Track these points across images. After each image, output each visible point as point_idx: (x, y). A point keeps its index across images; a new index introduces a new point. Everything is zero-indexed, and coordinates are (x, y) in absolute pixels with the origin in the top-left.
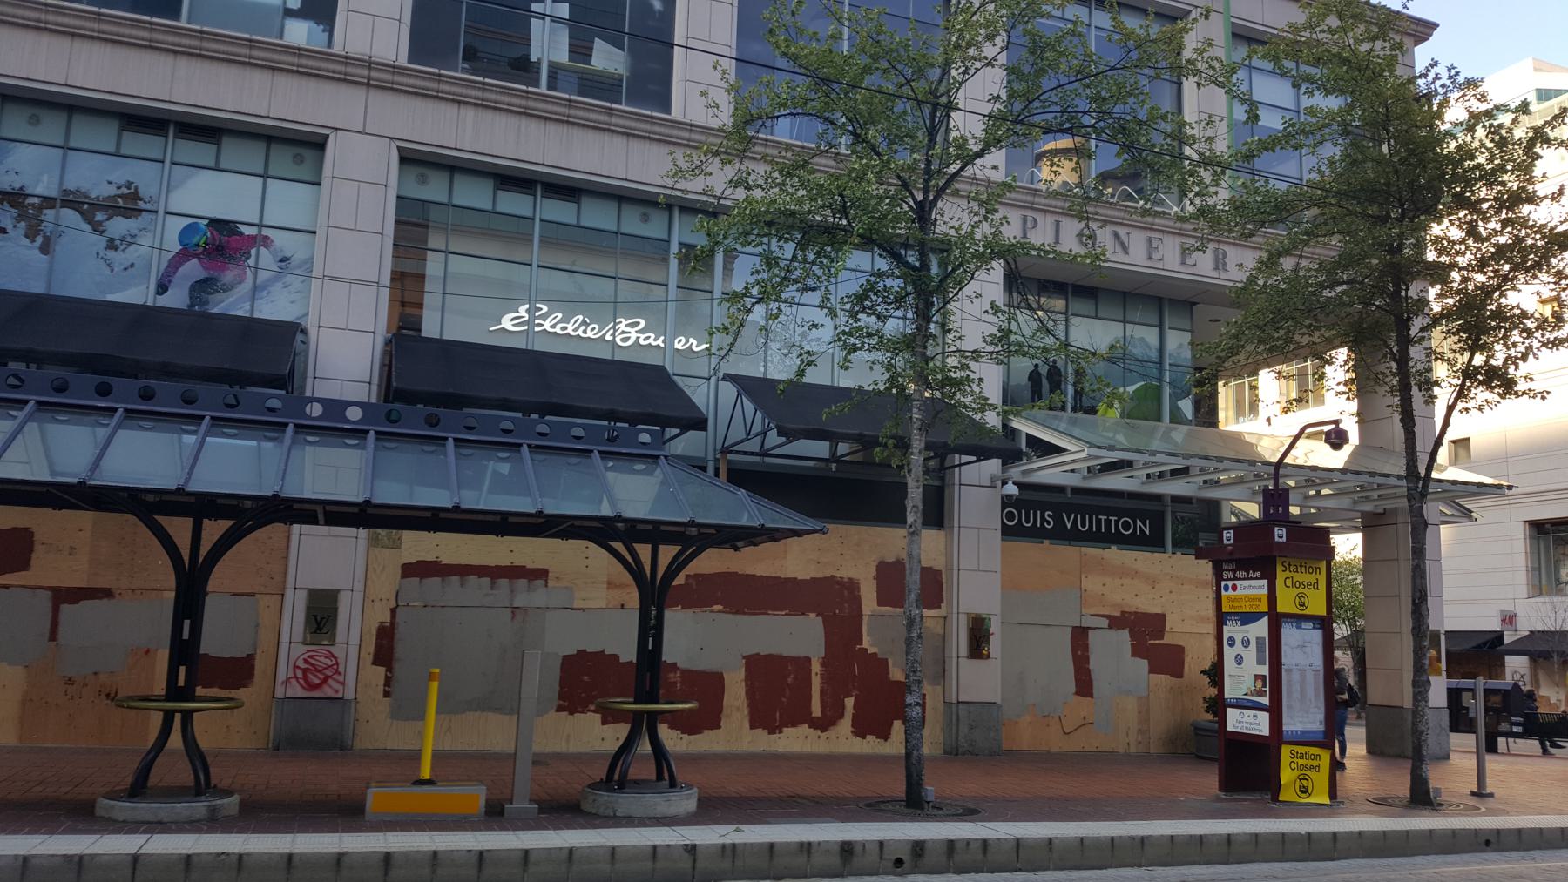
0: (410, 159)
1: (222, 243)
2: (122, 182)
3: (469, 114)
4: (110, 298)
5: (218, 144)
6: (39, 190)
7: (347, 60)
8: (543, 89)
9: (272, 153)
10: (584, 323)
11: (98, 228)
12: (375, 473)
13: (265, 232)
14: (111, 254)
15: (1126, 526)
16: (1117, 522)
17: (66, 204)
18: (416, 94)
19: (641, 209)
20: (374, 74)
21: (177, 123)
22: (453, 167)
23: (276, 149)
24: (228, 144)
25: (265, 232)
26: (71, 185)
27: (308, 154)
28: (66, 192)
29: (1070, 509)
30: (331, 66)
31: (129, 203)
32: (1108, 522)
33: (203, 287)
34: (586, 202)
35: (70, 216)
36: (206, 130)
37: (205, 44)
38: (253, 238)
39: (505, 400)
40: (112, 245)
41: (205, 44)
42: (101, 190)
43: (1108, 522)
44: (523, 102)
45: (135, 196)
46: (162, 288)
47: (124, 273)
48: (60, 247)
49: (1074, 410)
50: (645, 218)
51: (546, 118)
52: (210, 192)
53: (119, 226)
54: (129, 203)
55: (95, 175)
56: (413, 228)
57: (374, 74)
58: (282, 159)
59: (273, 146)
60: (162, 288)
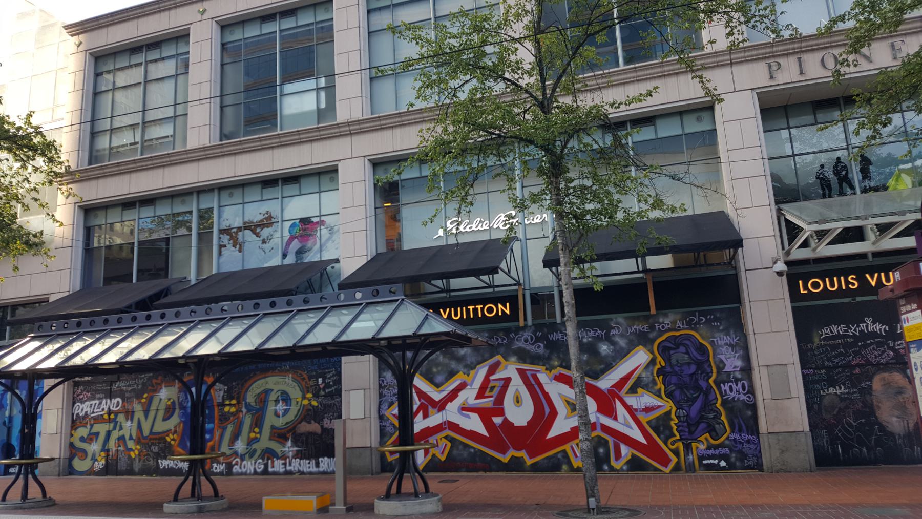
0: (377, 164)
1: (306, 227)
2: (265, 212)
3: (398, 131)
4: (266, 265)
5: (654, 125)
6: (236, 225)
7: (349, 124)
8: (622, 66)
9: (685, 122)
10: (481, 222)
11: (258, 235)
12: (218, 341)
13: (323, 218)
14: (264, 245)
15: (816, 285)
16: (482, 309)
17: (246, 228)
18: (655, 77)
19: (228, 191)
20: (351, 128)
21: (630, 121)
22: (397, 160)
23: (686, 118)
24: (303, 181)
25: (323, 218)
26: (246, 220)
27: (705, 115)
28: (245, 223)
29: (872, 270)
30: (333, 131)
31: (268, 221)
32: (475, 310)
33: (300, 252)
34: (660, 123)
35: (248, 232)
36: (292, 179)
37: (282, 140)
38: (317, 223)
39: (389, 279)
40: (264, 242)
41: (282, 140)
42: (257, 218)
43: (475, 310)
44: (421, 116)
45: (271, 217)
46: (284, 256)
47: (266, 254)
48: (246, 247)
49: (865, 190)
50: (699, 119)
51: (624, 83)
52: (300, 206)
53: (266, 232)
54: (268, 221)
55: (254, 212)
56: (388, 193)
57: (351, 128)
58: (325, 179)
59: (322, 177)
60: (284, 256)
